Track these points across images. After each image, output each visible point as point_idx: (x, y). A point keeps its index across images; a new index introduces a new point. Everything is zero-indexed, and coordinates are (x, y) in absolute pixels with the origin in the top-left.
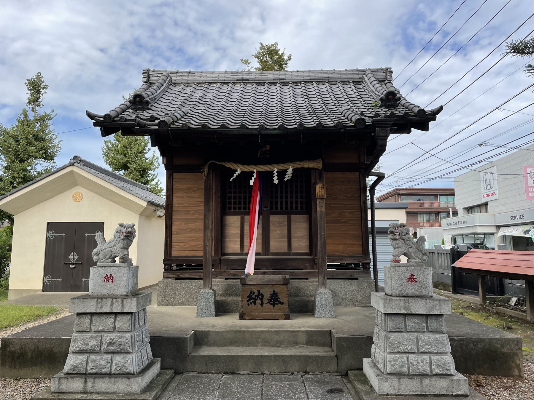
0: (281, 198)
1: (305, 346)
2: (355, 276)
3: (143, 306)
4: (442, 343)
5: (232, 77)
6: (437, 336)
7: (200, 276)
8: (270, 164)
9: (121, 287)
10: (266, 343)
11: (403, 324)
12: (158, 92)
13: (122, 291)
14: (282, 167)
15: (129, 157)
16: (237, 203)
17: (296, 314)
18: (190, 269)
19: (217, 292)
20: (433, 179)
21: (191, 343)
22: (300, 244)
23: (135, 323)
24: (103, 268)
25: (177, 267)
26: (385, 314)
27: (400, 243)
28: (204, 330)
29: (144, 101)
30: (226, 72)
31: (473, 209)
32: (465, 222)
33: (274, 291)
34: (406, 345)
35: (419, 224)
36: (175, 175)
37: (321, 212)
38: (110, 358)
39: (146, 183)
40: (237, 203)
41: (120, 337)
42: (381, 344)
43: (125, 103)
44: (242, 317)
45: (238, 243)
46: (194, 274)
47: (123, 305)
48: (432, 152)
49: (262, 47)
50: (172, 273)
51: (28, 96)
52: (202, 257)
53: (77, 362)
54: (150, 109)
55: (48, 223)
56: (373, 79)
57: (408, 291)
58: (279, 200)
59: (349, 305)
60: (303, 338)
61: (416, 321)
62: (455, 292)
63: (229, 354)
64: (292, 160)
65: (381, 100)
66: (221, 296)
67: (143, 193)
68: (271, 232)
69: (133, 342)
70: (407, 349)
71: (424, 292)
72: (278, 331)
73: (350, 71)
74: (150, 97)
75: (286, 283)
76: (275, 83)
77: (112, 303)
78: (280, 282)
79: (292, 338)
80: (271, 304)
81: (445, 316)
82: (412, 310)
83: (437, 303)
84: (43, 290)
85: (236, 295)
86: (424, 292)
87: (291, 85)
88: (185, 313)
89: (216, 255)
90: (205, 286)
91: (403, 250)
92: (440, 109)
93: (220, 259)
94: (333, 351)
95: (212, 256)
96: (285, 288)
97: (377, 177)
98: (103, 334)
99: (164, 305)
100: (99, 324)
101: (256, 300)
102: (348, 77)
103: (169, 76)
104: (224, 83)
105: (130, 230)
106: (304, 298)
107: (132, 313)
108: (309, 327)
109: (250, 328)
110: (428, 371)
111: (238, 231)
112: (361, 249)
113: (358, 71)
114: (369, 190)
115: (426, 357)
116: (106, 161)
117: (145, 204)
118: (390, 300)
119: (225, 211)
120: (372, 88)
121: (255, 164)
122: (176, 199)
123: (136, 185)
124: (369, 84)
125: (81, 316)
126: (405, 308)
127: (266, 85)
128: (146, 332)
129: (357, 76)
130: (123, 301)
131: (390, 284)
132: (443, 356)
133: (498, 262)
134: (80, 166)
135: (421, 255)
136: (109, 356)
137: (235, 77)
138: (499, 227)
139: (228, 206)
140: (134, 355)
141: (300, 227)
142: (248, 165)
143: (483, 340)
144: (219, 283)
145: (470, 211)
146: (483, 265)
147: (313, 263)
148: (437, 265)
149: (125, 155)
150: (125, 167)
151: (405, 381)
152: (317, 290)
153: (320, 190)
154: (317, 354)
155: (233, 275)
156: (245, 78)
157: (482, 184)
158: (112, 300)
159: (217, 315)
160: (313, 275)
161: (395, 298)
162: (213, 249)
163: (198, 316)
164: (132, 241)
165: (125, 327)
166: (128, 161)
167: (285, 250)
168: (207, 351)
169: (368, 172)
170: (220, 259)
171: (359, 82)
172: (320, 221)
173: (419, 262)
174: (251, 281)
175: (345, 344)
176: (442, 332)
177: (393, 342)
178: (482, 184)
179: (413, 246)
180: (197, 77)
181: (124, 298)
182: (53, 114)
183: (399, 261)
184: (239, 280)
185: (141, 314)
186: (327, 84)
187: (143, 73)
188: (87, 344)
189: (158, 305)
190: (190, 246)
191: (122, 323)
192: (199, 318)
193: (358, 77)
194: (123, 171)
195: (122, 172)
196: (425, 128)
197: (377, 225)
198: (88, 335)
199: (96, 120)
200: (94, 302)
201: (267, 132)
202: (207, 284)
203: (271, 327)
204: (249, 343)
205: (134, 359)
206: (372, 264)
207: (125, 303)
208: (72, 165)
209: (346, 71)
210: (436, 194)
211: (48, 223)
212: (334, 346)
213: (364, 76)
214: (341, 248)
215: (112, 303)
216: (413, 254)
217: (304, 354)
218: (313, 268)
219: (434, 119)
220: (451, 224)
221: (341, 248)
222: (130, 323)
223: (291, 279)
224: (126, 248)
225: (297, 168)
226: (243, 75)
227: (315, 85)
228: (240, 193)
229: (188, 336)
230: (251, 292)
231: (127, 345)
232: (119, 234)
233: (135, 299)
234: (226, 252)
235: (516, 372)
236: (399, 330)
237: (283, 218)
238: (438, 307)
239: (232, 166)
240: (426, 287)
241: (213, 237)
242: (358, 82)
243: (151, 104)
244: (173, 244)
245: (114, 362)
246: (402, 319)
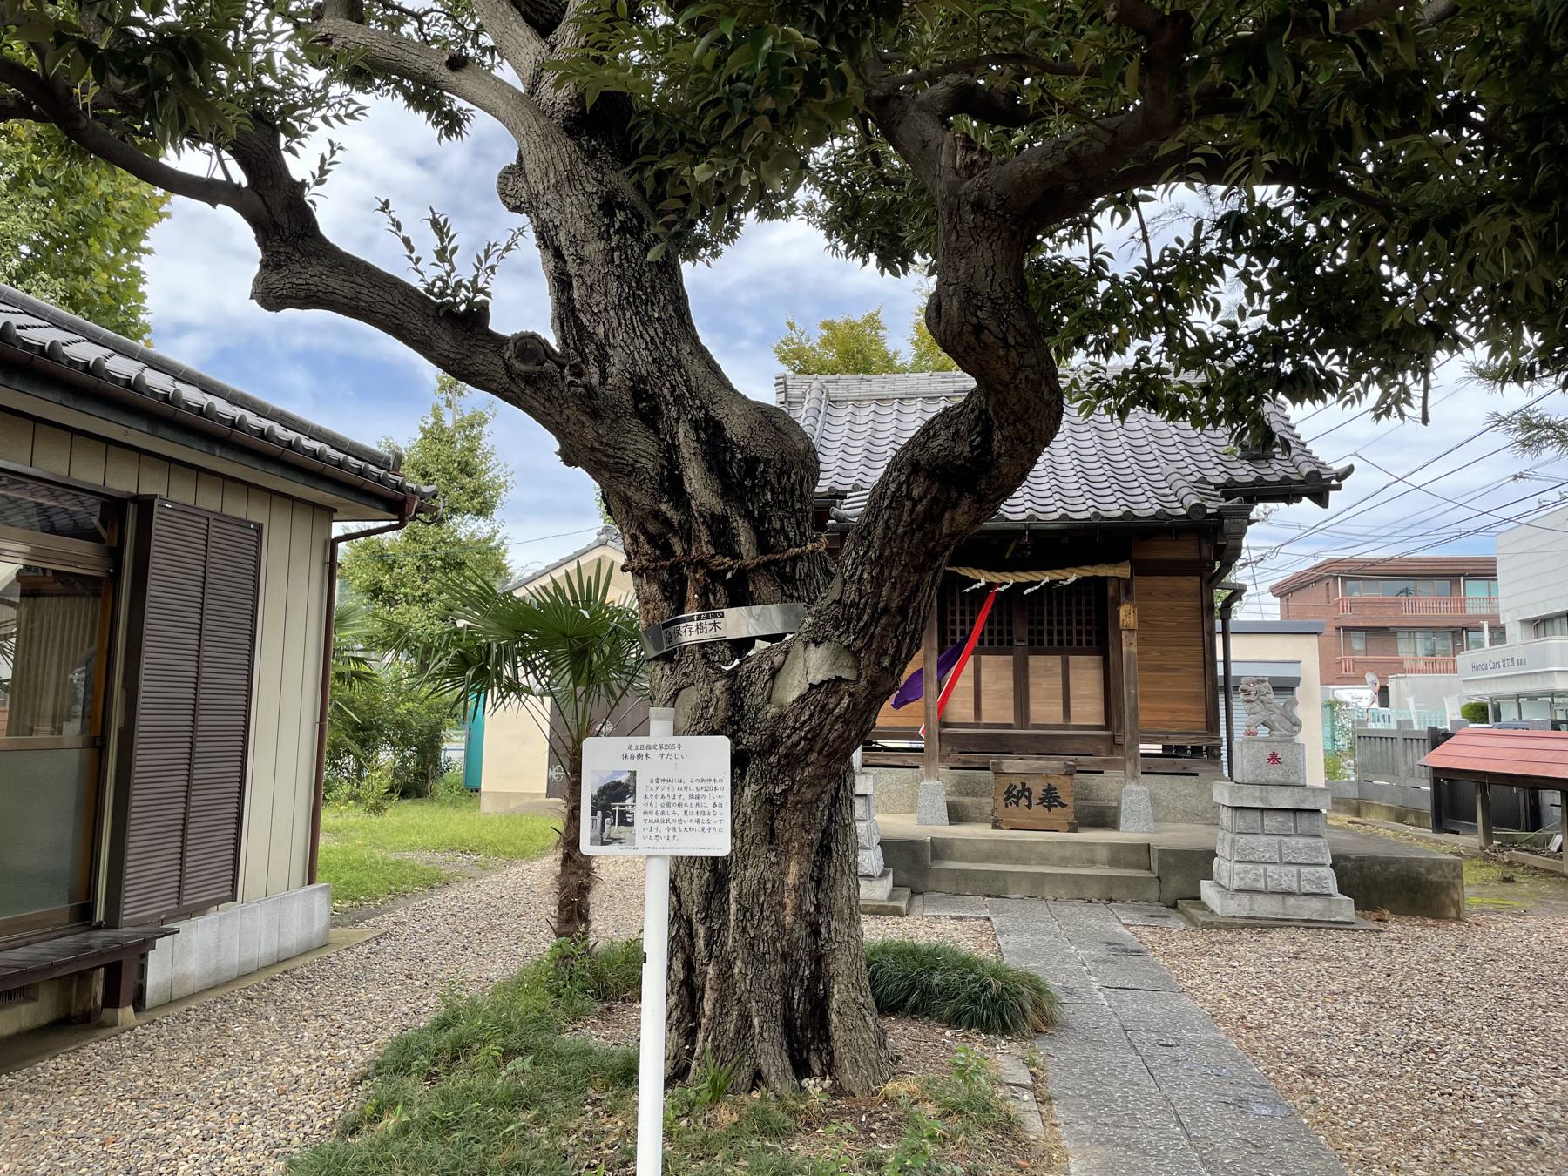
0: (1050, 623)
4: (1317, 850)
6: (1311, 841)
8: (1037, 569)
10: (1044, 859)
22: (1088, 709)
27: (1257, 707)
31: (1549, 625)
32: (1521, 662)
35: (1401, 662)
37: (1129, 653)
59: (1180, 821)
62: (1439, 826)
79: (1088, 854)
96: (1067, 779)
110: (1295, 888)
115: (1293, 869)
126: (1261, 800)
133: (1507, 754)
142: (998, 571)
143: (1397, 860)
145: (1542, 628)
147: (1114, 745)
148: (1403, 768)
151: (1259, 898)
153: (1127, 615)
155: (965, 762)
160: (1114, 765)
169: (1214, 580)
175: (1171, 860)
183: (1254, 734)
196: (1321, 498)
197: (1235, 671)
210: (1455, 574)
212: (1155, 865)
214: (1165, 717)
220: (1483, 667)
235: (1453, 913)
237: (1054, 661)
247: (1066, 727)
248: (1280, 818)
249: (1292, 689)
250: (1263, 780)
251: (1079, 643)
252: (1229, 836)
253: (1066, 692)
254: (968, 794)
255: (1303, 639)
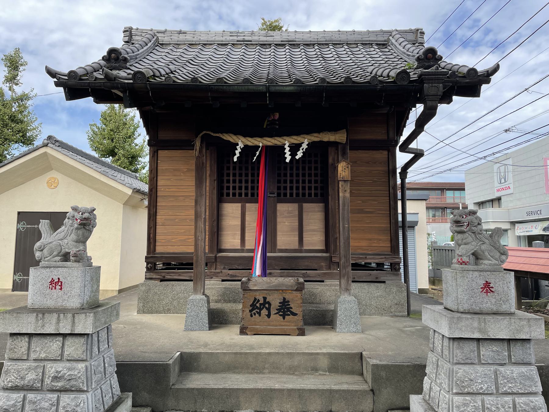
1: (328, 373)
2: (382, 279)
3: (105, 323)
5: (231, 38)
7: (191, 276)
8: (280, 136)
9: (73, 295)
11: (476, 353)
12: (140, 51)
13: (74, 303)
14: (295, 140)
15: (116, 143)
16: (237, 188)
17: (311, 327)
18: (179, 269)
19: (211, 298)
20: (441, 172)
21: (174, 370)
22: (315, 239)
23: (92, 348)
24: (48, 270)
25: (164, 266)
26: (450, 338)
27: (469, 237)
28: (193, 351)
29: (121, 58)
30: (224, 31)
31: (484, 205)
33: (284, 299)
34: (481, 383)
36: (160, 152)
37: (344, 197)
38: (55, 399)
39: (136, 171)
40: (237, 188)
41: (69, 369)
42: (443, 379)
43: (99, 62)
44: (243, 332)
45: (239, 237)
46: (184, 275)
47: (73, 322)
48: (447, 142)
49: (264, 23)
50: (156, 273)
51: (6, 73)
52: (192, 253)
53: (9, 403)
54: (129, 69)
55: (19, 213)
56: (402, 40)
57: (481, 306)
58: (288, 185)
59: (374, 314)
60: (324, 363)
61: (495, 348)
63: (227, 386)
64: (308, 132)
65: (418, 59)
66: (216, 302)
67: (128, 180)
68: (278, 223)
69: (89, 376)
70: (481, 388)
71: (504, 306)
72: (291, 353)
73: (373, 32)
74: (129, 55)
75: (300, 288)
76: (283, 45)
77: (59, 320)
78: (292, 286)
79: (310, 364)
80: (280, 315)
81: (532, 343)
82: (489, 333)
83: (525, 323)
84: (13, 290)
85: (235, 301)
86: (504, 306)
87: (302, 47)
88: (167, 329)
89: (211, 251)
90: (195, 291)
91: (473, 247)
92: (496, 69)
93: (216, 257)
94: (366, 382)
95: (205, 253)
96: (298, 294)
97: (413, 155)
98: (46, 363)
99: (146, 313)
100: (40, 348)
101: (261, 309)
102: (371, 39)
103: (155, 35)
104: (222, 45)
105: (86, 215)
106: (320, 306)
107: (88, 335)
108: (331, 347)
109: (253, 349)
111: (238, 222)
112: (389, 245)
113: (383, 32)
114: (399, 173)
115: (509, 399)
116: (91, 147)
117: (129, 192)
118: (459, 318)
119: (222, 196)
120: (403, 50)
121: (261, 136)
122: (161, 182)
123: (124, 173)
124: (398, 46)
125: (15, 337)
126: (480, 331)
127: (273, 47)
128: (110, 358)
129: (381, 38)
130: (74, 317)
131: (455, 295)
132: (532, 398)
134: (54, 147)
135: (498, 254)
136: (54, 396)
137: (235, 38)
138: (513, 223)
139: (225, 191)
140: (89, 395)
141: (314, 216)
142: (252, 137)
144: (214, 286)
146: (522, 265)
149: (112, 140)
150: (112, 153)
152: (339, 297)
153: (343, 170)
154: (345, 387)
155: (232, 276)
156: (247, 38)
157: (495, 178)
158: (59, 316)
159: (211, 328)
160: (331, 276)
161: (464, 316)
162: (207, 243)
163: (186, 330)
164: (90, 232)
165: (77, 354)
166: (115, 146)
167: (296, 246)
168: (197, 381)
170: (216, 257)
171: (384, 45)
172: (343, 210)
173: (495, 265)
174: (255, 285)
175: (383, 374)
176: (530, 364)
177: (462, 379)
178: (495, 178)
179: (487, 241)
180: (189, 37)
181: (75, 312)
182: (33, 94)
184: (239, 283)
185: (103, 335)
186: (346, 47)
187: (124, 32)
188: (22, 378)
189: (139, 312)
190: (179, 238)
191: (73, 348)
192: (188, 332)
193: (383, 39)
194: (111, 157)
195: (109, 160)
198: (25, 365)
199: (59, 79)
200: (32, 318)
201: (278, 88)
202: (199, 287)
203: (282, 347)
204: (253, 369)
205: (90, 400)
206: (402, 264)
207: (76, 321)
208: (46, 145)
209: (369, 32)
211: (19, 213)
212: (368, 376)
213: (391, 38)
214: (364, 244)
215: (59, 320)
216: (487, 254)
217: (327, 387)
218: (330, 268)
219: (488, 82)
221: (364, 244)
222: (84, 348)
223: (305, 281)
224: (83, 241)
225: (314, 142)
226: (244, 36)
227: (331, 47)
228: (240, 175)
229: (171, 362)
230: (255, 299)
231: (80, 380)
232: (71, 222)
233: (92, 315)
234: (223, 248)
236: (470, 361)
238: (526, 329)
239: (230, 138)
240: (508, 300)
241: (207, 229)
242: (383, 45)
243: (131, 64)
244: (158, 238)
245: (62, 404)
246: (475, 344)
247: (300, 251)
248: (495, 347)
249: (413, 227)
250: (477, 309)
251: (310, 195)
252: (447, 366)
253: (299, 227)
254: (230, 301)
255: (419, 202)
